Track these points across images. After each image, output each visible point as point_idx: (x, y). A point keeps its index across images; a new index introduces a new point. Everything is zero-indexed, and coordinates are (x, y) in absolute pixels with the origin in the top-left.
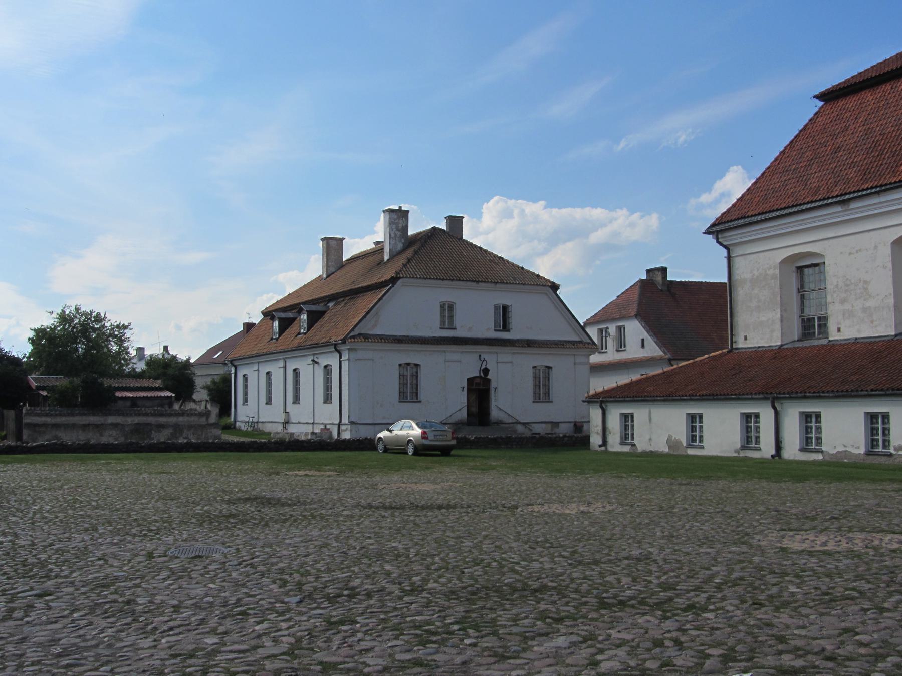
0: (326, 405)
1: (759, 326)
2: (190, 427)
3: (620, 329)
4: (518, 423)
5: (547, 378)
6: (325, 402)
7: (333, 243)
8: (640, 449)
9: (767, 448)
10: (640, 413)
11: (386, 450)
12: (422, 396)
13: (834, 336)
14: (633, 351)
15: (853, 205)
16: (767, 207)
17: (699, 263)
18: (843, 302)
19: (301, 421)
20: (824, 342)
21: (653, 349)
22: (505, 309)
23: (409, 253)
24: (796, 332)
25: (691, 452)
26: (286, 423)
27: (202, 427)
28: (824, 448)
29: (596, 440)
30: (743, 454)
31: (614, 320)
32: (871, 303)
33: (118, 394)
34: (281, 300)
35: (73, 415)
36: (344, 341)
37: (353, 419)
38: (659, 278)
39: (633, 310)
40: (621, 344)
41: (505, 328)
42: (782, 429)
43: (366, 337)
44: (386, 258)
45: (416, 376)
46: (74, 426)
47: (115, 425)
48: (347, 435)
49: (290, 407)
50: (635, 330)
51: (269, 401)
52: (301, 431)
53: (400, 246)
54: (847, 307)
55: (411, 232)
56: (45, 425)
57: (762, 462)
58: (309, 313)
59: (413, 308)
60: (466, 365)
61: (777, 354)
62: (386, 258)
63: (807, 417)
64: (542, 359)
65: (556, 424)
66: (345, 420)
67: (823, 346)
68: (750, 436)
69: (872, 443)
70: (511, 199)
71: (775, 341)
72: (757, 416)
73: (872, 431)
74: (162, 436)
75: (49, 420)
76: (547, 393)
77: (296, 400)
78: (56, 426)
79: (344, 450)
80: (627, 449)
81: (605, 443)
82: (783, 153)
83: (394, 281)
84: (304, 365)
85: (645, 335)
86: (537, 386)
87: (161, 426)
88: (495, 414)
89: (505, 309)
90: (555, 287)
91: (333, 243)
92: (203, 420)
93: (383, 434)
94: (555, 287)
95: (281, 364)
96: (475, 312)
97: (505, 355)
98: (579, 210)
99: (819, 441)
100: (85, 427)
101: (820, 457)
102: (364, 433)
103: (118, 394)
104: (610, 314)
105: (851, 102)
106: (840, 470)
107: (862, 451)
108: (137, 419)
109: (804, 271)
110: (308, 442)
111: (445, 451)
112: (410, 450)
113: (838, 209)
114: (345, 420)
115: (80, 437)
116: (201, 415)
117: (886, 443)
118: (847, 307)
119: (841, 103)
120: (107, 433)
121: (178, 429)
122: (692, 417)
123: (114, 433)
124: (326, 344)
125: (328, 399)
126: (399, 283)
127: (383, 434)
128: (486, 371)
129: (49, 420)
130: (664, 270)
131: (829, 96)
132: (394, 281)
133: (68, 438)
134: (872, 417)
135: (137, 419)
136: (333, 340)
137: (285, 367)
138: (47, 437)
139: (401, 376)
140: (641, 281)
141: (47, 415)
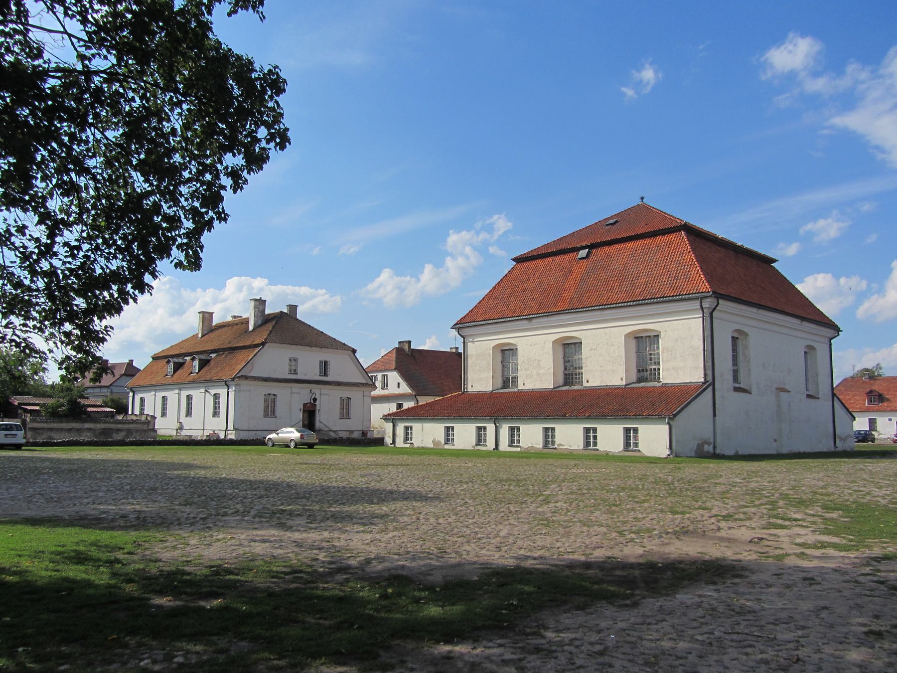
0: (188, 418)
1: (480, 378)
2: (137, 431)
3: (384, 376)
4: (331, 431)
5: (348, 405)
6: (214, 416)
7: (207, 315)
8: (416, 446)
9: (490, 444)
10: (417, 426)
11: (273, 445)
12: (278, 413)
13: (521, 387)
14: (392, 390)
15: (534, 321)
16: (487, 317)
17: (436, 339)
18: (526, 370)
19: (717, 418)
20: (516, 390)
21: (405, 389)
22: (326, 363)
23: (269, 326)
24: (499, 383)
25: (446, 447)
26: (181, 428)
27: (145, 431)
28: (521, 445)
29: (388, 440)
30: (477, 448)
31: (380, 371)
32: (541, 371)
33: (89, 409)
34: (167, 350)
35: (61, 422)
36: (233, 379)
37: (236, 427)
38: (406, 347)
39: (393, 365)
40: (385, 385)
41: (325, 374)
42: (496, 435)
43: (246, 378)
44: (251, 328)
45: (274, 401)
46: (62, 430)
47: (89, 429)
48: (232, 436)
49: (183, 419)
50: (394, 377)
51: (216, 414)
52: (198, 435)
53: (260, 322)
54: (528, 372)
55: (266, 313)
56: (42, 429)
57: (488, 452)
58: (200, 360)
59: (274, 359)
60: (302, 395)
61: (491, 395)
62: (251, 328)
63: (512, 429)
64: (273, 388)
65: (352, 432)
66: (231, 427)
67: (515, 392)
68: (480, 440)
69: (546, 443)
70: (254, 278)
71: (488, 388)
72: (485, 428)
73: (546, 437)
74: (119, 437)
75: (45, 425)
76: (348, 413)
77: (189, 413)
78: (51, 429)
79: (245, 445)
80: (407, 445)
81: (394, 442)
82: (494, 288)
83: (263, 344)
84: (198, 394)
85: (401, 380)
86: (342, 408)
87: (119, 430)
88: (318, 425)
89: (326, 363)
90: (354, 351)
91: (207, 315)
92: (145, 427)
93: (273, 436)
94: (354, 351)
95: (177, 391)
96: (308, 362)
97: (325, 389)
98: (290, 287)
99: (519, 441)
100: (70, 430)
101: (519, 449)
102: (259, 436)
103: (89, 409)
104: (381, 366)
105: (531, 264)
106: (529, 455)
107: (541, 446)
108: (103, 426)
109: (507, 353)
110: (199, 441)
111: (311, 446)
112: (292, 445)
113: (526, 322)
114: (231, 427)
115: (67, 438)
116: (144, 423)
117: (553, 443)
118: (528, 372)
119: (526, 264)
120: (84, 434)
121: (129, 432)
122: (448, 429)
123: (88, 434)
124: (219, 381)
125: (216, 414)
126: (267, 345)
127: (273, 436)
128: (315, 400)
129: (45, 425)
130: (410, 342)
131: (519, 260)
132: (263, 344)
133: (58, 437)
134: (546, 430)
135: (103, 426)
136: (224, 378)
137: (179, 394)
138: (44, 436)
139: (266, 401)
140: (397, 348)
141: (44, 422)
